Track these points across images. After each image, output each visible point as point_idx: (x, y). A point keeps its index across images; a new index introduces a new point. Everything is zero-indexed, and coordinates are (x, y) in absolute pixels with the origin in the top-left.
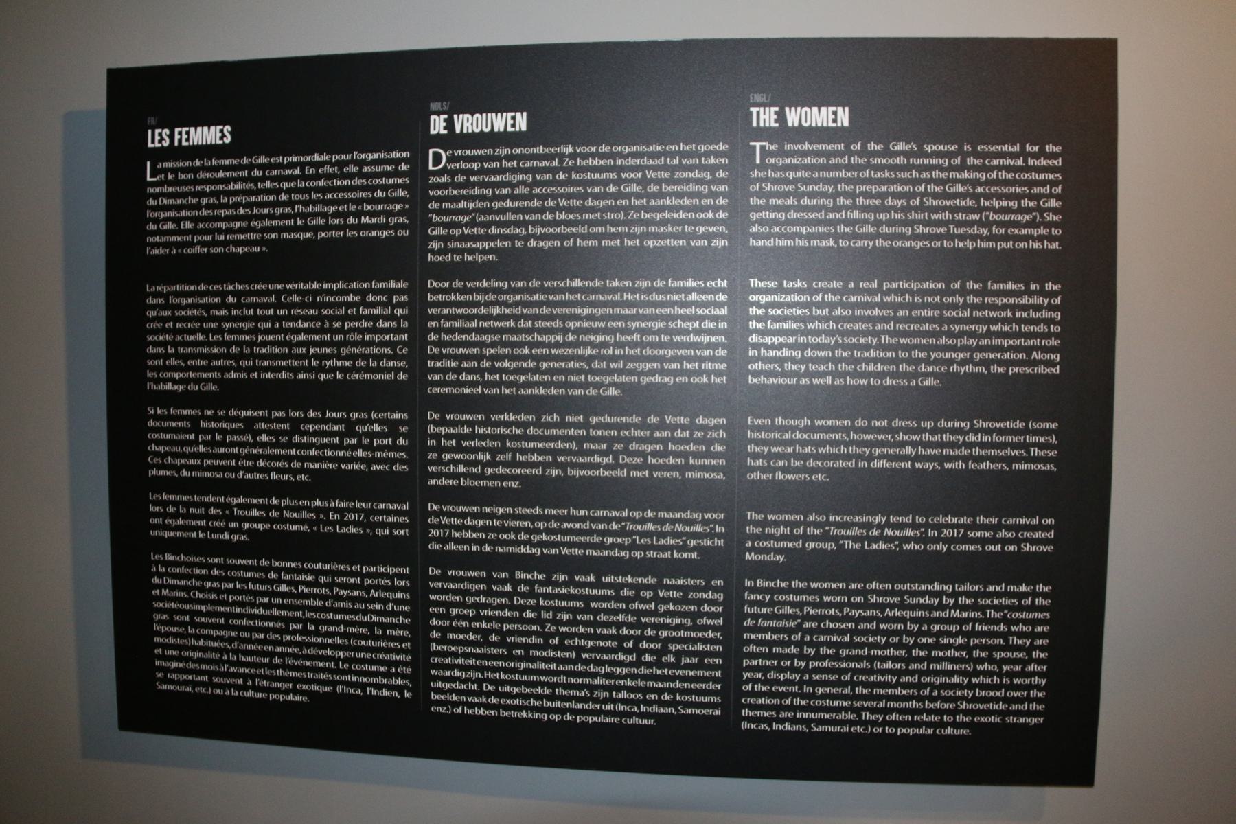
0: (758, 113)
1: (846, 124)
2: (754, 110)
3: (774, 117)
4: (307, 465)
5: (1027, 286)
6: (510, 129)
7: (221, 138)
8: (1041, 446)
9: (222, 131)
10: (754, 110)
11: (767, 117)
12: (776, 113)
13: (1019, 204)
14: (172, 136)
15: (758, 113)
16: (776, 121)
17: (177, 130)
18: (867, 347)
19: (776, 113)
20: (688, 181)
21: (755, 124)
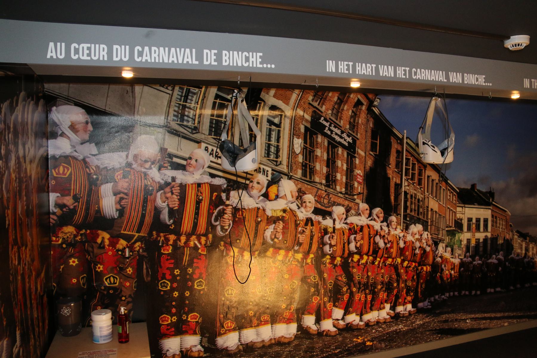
3: (214, 57)
11: (254, 60)
17: (115, 47)
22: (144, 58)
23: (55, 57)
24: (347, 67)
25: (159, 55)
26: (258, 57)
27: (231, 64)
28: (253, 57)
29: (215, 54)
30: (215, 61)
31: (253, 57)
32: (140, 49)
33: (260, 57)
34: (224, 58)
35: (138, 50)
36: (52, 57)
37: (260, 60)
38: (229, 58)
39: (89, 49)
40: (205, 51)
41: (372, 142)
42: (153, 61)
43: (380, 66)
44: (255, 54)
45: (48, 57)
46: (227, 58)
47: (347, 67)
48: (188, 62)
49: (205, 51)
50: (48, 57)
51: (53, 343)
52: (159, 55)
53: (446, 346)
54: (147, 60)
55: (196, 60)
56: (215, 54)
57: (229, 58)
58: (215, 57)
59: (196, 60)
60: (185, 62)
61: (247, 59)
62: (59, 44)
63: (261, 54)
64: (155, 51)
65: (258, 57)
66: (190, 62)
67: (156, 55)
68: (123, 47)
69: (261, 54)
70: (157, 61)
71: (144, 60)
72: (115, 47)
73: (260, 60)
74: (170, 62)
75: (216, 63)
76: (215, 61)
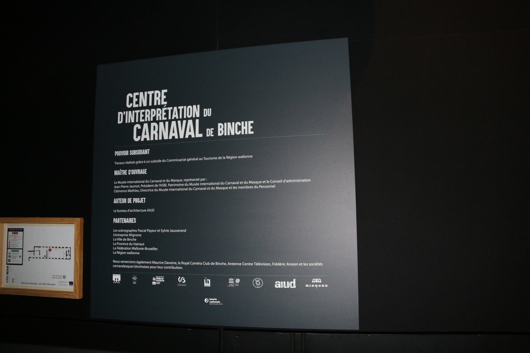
9: (144, 113)
11: (246, 128)
22: (143, 137)
24: (165, 114)
25: (158, 132)
26: (163, 111)
28: (244, 126)
30: (252, 130)
31: (244, 126)
32: (139, 127)
33: (252, 125)
34: (219, 129)
35: (137, 128)
37: (165, 97)
38: (224, 129)
39: (138, 97)
41: (220, 48)
46: (222, 129)
47: (165, 114)
48: (190, 136)
51: (204, 323)
52: (158, 132)
53: (354, 165)
55: (200, 133)
57: (224, 129)
58: (251, 127)
59: (200, 133)
60: (187, 137)
61: (240, 128)
63: (252, 122)
64: (154, 127)
65: (163, 111)
66: (193, 136)
67: (155, 132)
68: (225, 124)
69: (252, 122)
70: (156, 139)
71: (142, 140)
73: (165, 97)
74: (170, 138)
75: (252, 133)
76: (252, 130)
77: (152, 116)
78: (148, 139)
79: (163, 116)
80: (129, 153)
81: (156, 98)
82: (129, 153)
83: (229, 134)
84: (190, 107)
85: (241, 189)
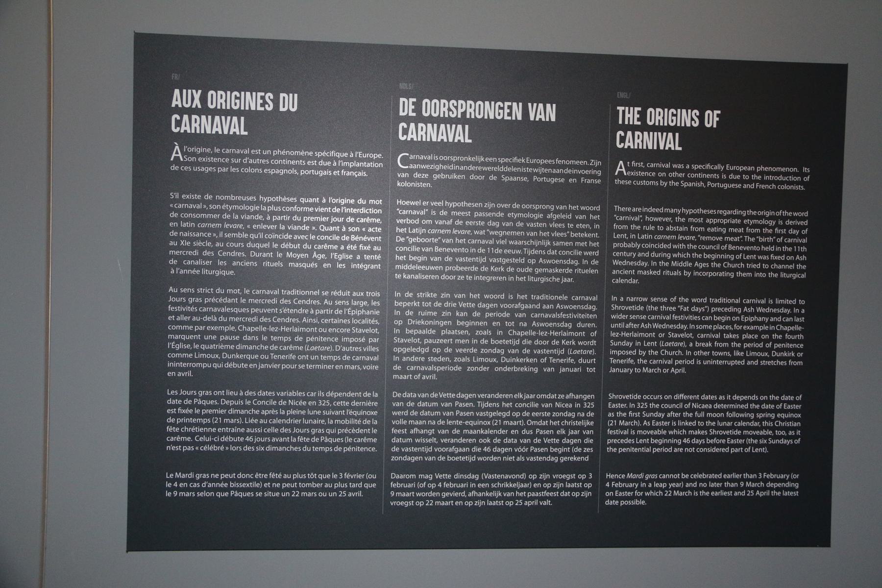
0: (624, 112)
1: (553, 119)
2: (620, 109)
3: (637, 116)
4: (639, 272)
5: (800, 169)
6: (507, 118)
7: (262, 105)
8: (792, 333)
9: (263, 98)
10: (620, 109)
11: (631, 116)
12: (639, 112)
13: (735, 275)
14: (276, 101)
15: (624, 112)
16: (638, 120)
17: (282, 95)
18: (659, 419)
19: (639, 112)
20: (234, 249)
21: (296, 95)
22: (627, 145)
23: (180, 106)
25: (200, 125)
26: (715, 115)
27: (242, 108)
29: (413, 103)
30: (413, 111)
33: (718, 115)
36: (177, 105)
37: (638, 116)
39: (510, 107)
40: (402, 100)
42: (193, 131)
43: (530, 104)
44: (632, 108)
45: (173, 105)
48: (235, 133)
49: (402, 100)
50: (173, 105)
52: (200, 125)
54: (185, 131)
56: (413, 103)
60: (231, 133)
62: (184, 91)
63: (719, 112)
65: (715, 115)
66: (238, 133)
68: (291, 95)
69: (719, 112)
71: (182, 131)
72: (282, 95)
73: (638, 116)
74: (214, 132)
76: (413, 111)
77: (460, 111)
78: (415, 139)
79: (506, 114)
80: (701, 118)
81: (627, 115)
82: (701, 118)
83: (203, 132)
84: (499, 118)
85: (268, 175)
